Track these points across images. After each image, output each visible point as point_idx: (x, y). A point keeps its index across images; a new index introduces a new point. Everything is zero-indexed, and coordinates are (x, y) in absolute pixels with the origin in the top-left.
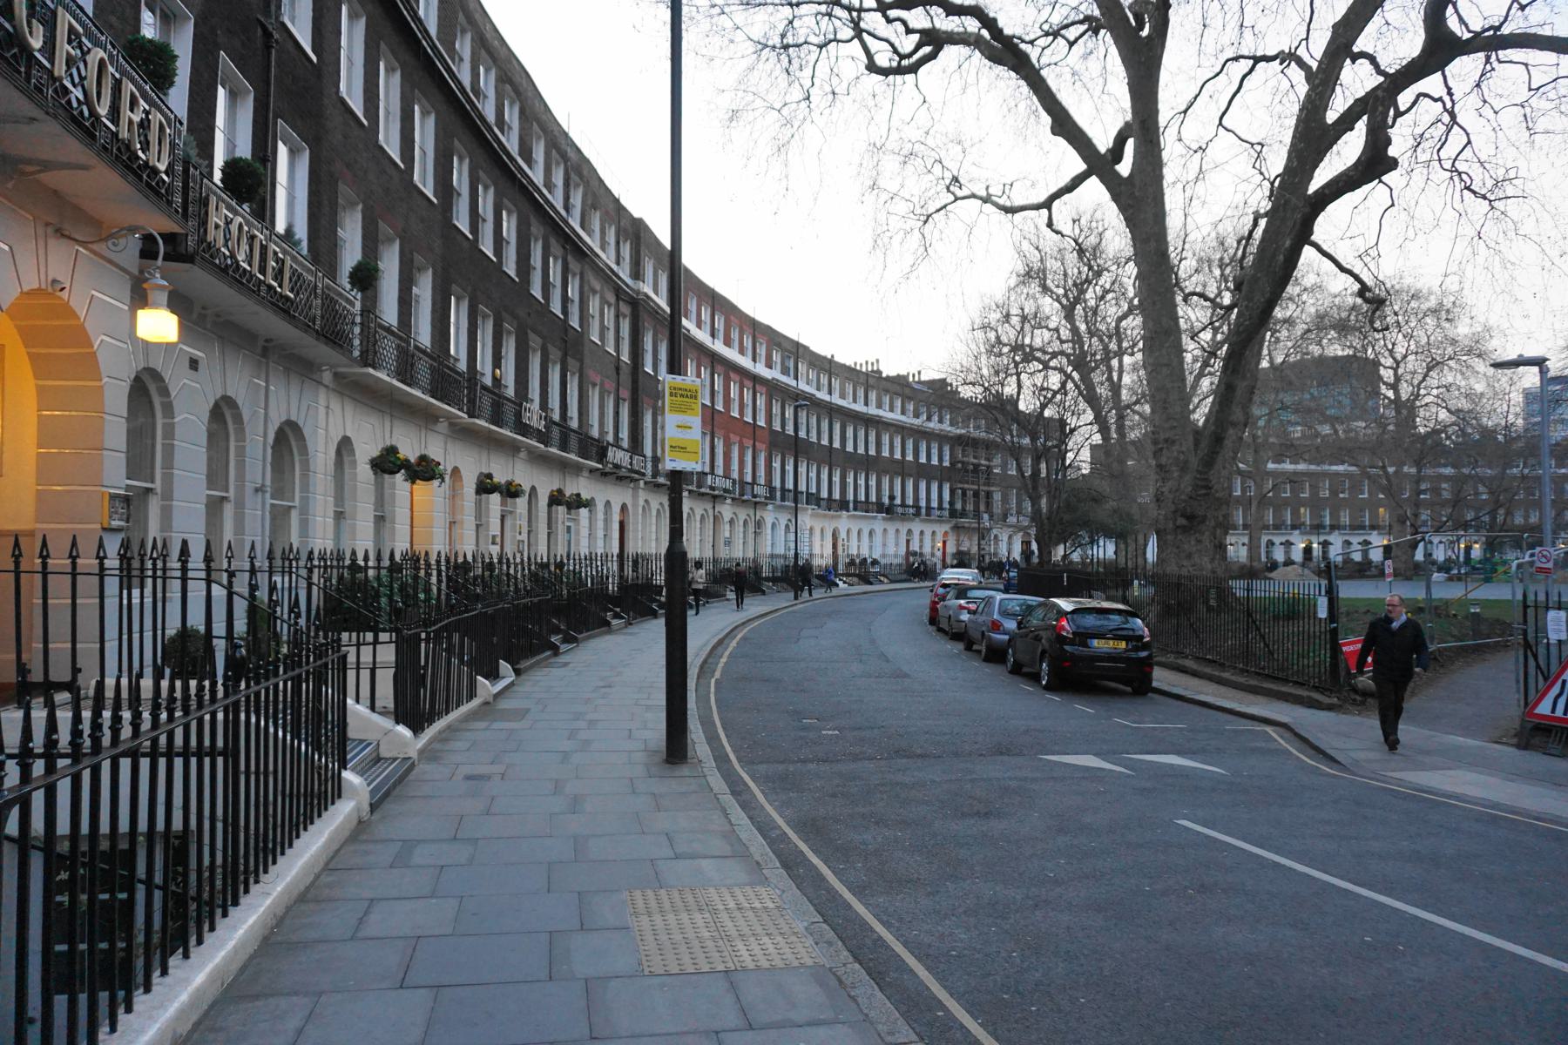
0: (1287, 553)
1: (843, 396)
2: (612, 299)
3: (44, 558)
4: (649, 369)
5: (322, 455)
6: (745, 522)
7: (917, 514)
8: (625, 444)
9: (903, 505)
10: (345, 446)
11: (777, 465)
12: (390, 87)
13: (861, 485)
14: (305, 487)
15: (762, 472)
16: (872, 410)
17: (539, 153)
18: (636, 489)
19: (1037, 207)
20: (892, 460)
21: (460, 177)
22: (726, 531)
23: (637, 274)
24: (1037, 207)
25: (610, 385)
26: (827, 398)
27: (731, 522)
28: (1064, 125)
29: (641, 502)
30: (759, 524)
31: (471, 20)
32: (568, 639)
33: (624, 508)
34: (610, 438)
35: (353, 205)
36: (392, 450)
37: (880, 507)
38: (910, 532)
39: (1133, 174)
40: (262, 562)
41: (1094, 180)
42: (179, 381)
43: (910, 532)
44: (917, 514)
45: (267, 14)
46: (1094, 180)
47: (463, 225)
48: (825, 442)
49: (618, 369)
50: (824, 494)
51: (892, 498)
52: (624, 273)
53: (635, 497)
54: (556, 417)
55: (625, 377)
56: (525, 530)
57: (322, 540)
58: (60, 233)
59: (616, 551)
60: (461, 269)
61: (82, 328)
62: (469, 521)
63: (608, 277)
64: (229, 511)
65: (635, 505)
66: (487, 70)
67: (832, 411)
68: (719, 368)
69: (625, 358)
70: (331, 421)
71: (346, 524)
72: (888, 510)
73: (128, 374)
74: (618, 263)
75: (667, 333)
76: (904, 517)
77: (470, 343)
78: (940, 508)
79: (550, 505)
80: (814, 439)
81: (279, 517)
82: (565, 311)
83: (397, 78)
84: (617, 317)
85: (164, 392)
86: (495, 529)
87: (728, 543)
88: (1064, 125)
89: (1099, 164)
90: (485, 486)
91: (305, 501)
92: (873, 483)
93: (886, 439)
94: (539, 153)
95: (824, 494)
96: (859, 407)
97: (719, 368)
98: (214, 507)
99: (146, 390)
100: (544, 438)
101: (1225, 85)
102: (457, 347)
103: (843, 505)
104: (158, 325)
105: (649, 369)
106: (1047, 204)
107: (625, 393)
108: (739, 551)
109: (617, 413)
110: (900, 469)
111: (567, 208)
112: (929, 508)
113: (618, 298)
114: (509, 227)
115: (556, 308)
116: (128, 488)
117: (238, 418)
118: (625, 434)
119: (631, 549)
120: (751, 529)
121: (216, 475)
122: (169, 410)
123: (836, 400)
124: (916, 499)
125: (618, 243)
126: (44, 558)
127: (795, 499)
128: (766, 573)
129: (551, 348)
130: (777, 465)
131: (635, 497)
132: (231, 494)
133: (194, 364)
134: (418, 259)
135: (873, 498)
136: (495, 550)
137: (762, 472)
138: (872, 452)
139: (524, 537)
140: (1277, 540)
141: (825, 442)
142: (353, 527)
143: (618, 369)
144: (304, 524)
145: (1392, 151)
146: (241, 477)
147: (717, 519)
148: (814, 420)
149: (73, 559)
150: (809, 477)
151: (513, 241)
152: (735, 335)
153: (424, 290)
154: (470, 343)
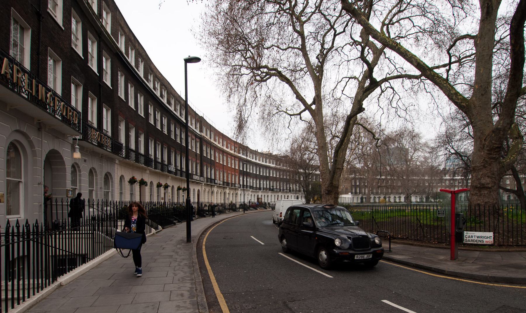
0: (400, 200)
1: (259, 161)
2: (194, 137)
3: (56, 202)
4: (205, 155)
5: (117, 180)
6: (221, 193)
7: (280, 191)
8: (199, 175)
9: (276, 188)
10: (122, 178)
11: (241, 179)
12: (131, 91)
13: (265, 184)
14: (112, 187)
15: (237, 181)
16: (268, 164)
17: (173, 102)
18: (202, 186)
19: (297, 115)
20: (273, 177)
21: (151, 110)
22: (227, 196)
23: (201, 131)
24: (297, 115)
25: (194, 160)
26: (255, 161)
27: (229, 194)
28: (299, 97)
29: (203, 189)
30: (237, 194)
31: (152, 71)
32: (179, 222)
33: (199, 191)
34: (195, 173)
35: (123, 121)
36: (133, 178)
37: (270, 189)
38: (278, 196)
39: (316, 108)
40: (100, 203)
41: (307, 111)
42: (82, 165)
43: (278, 196)
44: (280, 191)
45: (100, 81)
46: (307, 111)
47: (152, 122)
48: (255, 173)
49: (196, 155)
50: (255, 186)
51: (273, 187)
52: (198, 131)
53: (202, 187)
54: (179, 168)
55: (198, 157)
56: (171, 196)
57: (117, 199)
58: (57, 138)
59: (196, 201)
60: (151, 133)
61: (61, 156)
62: (155, 194)
63: (193, 133)
64: (94, 193)
65: (202, 190)
66: (158, 83)
67: (256, 165)
68: (225, 154)
69: (198, 152)
70: (118, 172)
71: (123, 196)
72: (272, 190)
73: (71, 164)
74: (196, 128)
75: (185, 155)
76: (277, 192)
77: (155, 151)
78: (286, 189)
79: (178, 190)
80: (251, 172)
81: (106, 194)
82: (181, 141)
83: (133, 89)
84: (196, 142)
85: (79, 167)
86: (162, 196)
87: (228, 199)
88: (299, 97)
89: (307, 107)
90: (159, 185)
91: (112, 190)
92: (268, 183)
93: (271, 172)
94: (173, 102)
95: (255, 186)
96: (264, 163)
97: (225, 154)
98: (91, 192)
99: (75, 167)
100: (176, 174)
101: (343, 83)
102: (151, 152)
103: (260, 189)
104: (77, 155)
105: (205, 155)
106: (300, 114)
107: (198, 161)
108: (205, 199)
109: (196, 167)
110: (275, 179)
111: (181, 115)
112: (283, 189)
113: (196, 137)
114: (165, 121)
115: (178, 141)
116: (72, 188)
117: (96, 172)
118: (199, 171)
119: (201, 201)
120: (234, 195)
121: (91, 184)
122: (80, 171)
123: (257, 161)
124: (280, 187)
125: (195, 123)
126: (56, 202)
127: (245, 187)
128: (238, 206)
129: (177, 151)
130: (241, 179)
131: (202, 187)
132: (95, 189)
133: (85, 161)
134: (140, 132)
135: (268, 187)
136: (163, 201)
137: (237, 181)
138: (268, 175)
139: (171, 198)
140: (397, 196)
141: (255, 173)
142: (125, 196)
143: (196, 155)
144: (112, 195)
145: (363, 106)
146: (97, 185)
147: (225, 193)
148: (251, 167)
149: (62, 202)
150: (250, 181)
151: (166, 124)
152: (229, 146)
153: (142, 139)
154: (155, 151)
